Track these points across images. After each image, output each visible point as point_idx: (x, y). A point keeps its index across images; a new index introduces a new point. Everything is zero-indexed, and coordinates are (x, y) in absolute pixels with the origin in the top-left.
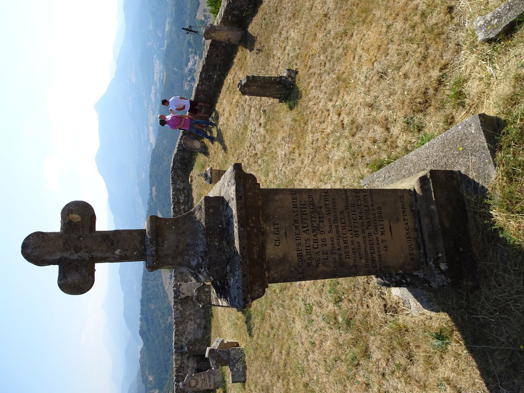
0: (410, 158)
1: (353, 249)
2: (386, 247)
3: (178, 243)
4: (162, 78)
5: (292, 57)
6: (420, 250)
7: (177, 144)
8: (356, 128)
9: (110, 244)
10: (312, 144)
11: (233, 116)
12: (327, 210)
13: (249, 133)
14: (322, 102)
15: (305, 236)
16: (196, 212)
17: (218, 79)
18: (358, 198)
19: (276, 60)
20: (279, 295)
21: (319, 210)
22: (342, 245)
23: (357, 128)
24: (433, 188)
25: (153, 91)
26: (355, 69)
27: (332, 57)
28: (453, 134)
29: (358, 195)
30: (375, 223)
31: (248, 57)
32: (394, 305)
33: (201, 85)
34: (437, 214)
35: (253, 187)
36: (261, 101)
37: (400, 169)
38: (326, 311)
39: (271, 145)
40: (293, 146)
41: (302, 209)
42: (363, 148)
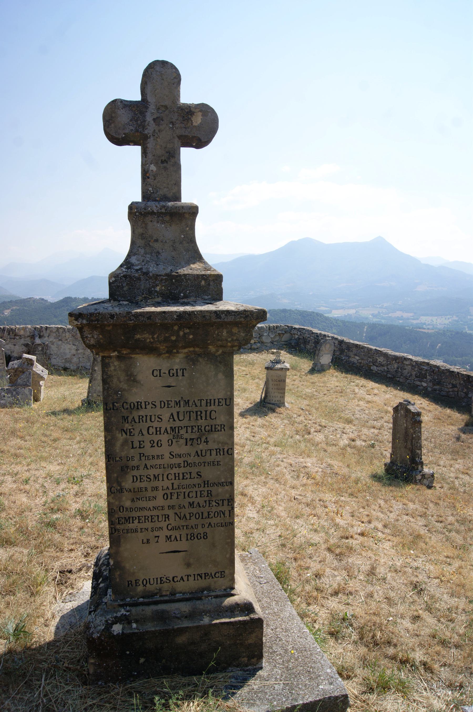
0: (287, 609)
1: (146, 489)
2: (148, 541)
3: (162, 242)
4: (424, 326)
5: (453, 482)
6: (143, 598)
7: (326, 333)
8: (340, 552)
9: (163, 158)
10: (320, 500)
11: (366, 405)
12: (204, 452)
13: (341, 425)
14: (382, 516)
15: (166, 416)
16: (202, 265)
17: (421, 388)
18: (221, 503)
19: (448, 462)
20: (99, 450)
21: (203, 439)
22: (152, 472)
23: (341, 554)
24: (236, 622)
25: (405, 315)
26: (433, 557)
27: (450, 531)
28: (319, 662)
29: (226, 503)
30: (183, 526)
31: (453, 428)
32: (70, 581)
33: (411, 364)
34: (195, 625)
35: (235, 338)
36: (388, 442)
37: (271, 596)
38: (71, 499)
39: (322, 453)
40: (318, 477)
41: (204, 413)
42: (309, 561)
